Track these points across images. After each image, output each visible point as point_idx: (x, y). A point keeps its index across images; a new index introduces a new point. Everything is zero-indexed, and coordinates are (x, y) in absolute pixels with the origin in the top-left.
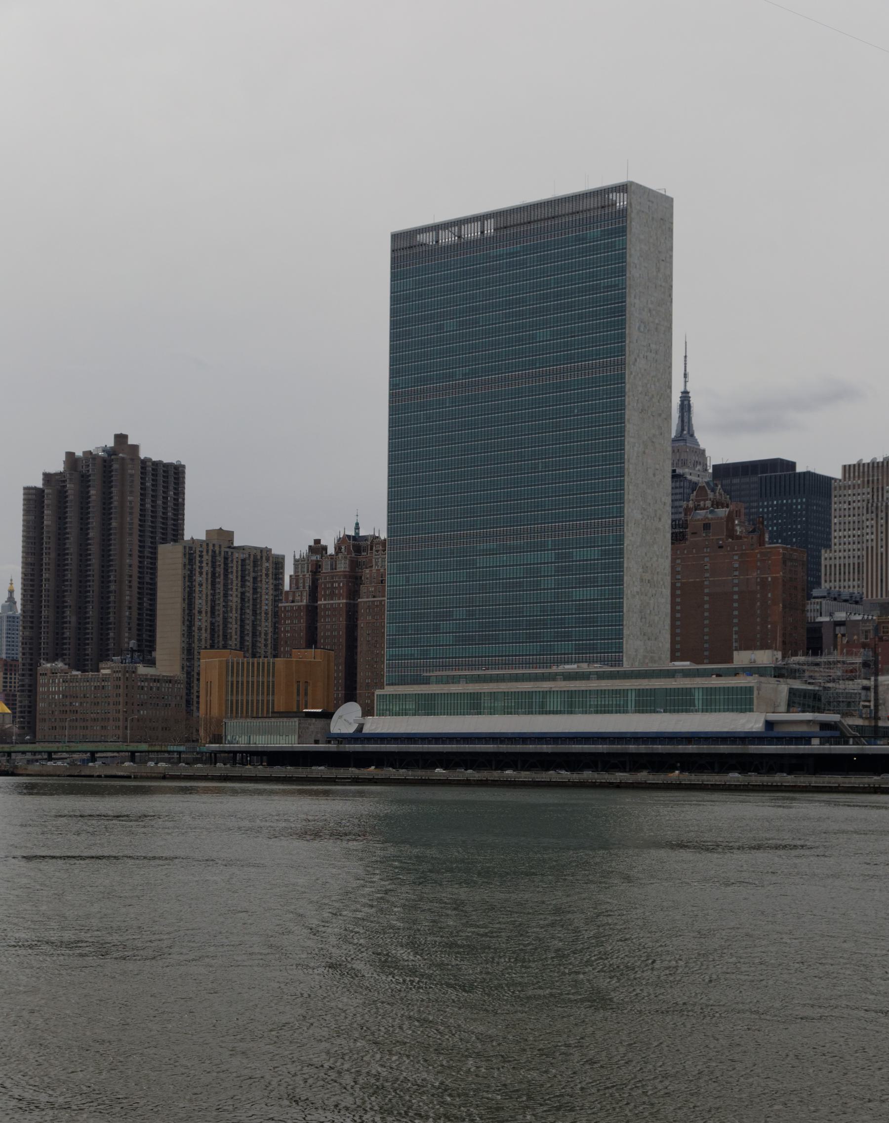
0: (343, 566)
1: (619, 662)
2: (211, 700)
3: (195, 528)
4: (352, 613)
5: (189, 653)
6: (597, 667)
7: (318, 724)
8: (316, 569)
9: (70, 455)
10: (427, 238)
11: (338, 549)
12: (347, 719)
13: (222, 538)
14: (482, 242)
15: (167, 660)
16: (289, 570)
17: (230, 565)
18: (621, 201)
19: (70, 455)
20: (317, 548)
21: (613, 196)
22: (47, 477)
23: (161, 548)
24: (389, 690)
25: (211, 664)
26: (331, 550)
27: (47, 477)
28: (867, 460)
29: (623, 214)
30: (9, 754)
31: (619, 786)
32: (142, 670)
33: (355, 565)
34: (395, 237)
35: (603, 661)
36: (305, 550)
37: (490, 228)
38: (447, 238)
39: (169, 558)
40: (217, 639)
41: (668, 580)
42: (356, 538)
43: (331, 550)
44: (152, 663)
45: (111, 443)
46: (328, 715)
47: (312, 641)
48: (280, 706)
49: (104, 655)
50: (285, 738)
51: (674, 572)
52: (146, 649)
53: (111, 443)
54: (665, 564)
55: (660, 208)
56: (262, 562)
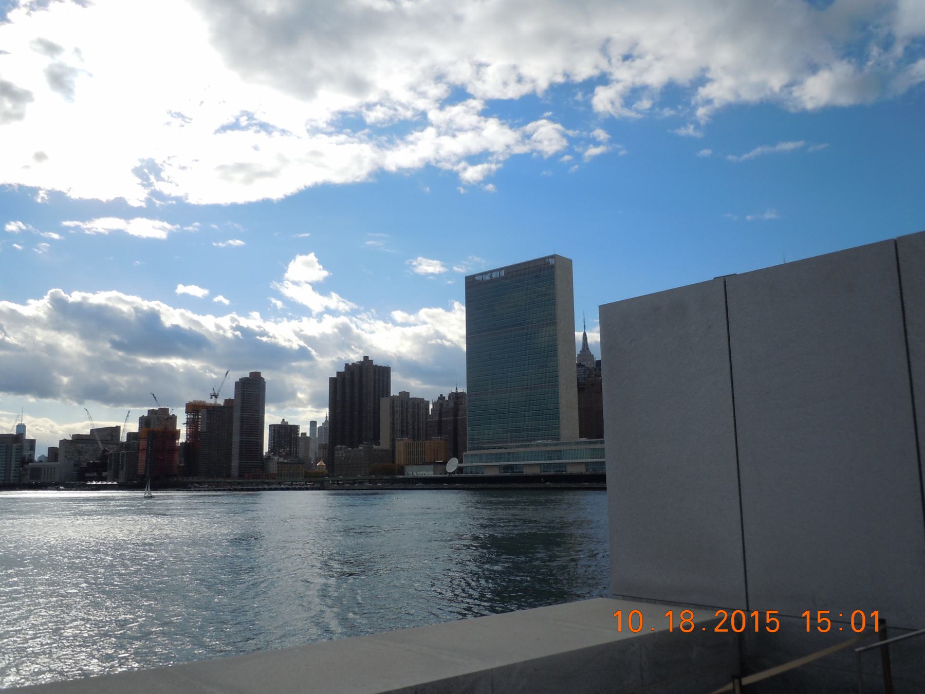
0: (452, 404)
1: (558, 439)
2: (400, 458)
3: (394, 392)
4: (455, 422)
5: (393, 441)
6: (550, 441)
7: (440, 467)
8: (441, 405)
9: (347, 365)
10: (479, 278)
11: (449, 397)
12: (452, 465)
13: (404, 395)
14: (500, 278)
15: (385, 443)
16: (431, 407)
17: (409, 406)
18: (552, 261)
19: (347, 365)
20: (441, 398)
21: (549, 260)
22: (338, 373)
23: (382, 399)
24: (468, 452)
25: (400, 445)
26: (447, 399)
27: (338, 373)
28: (302, 187)
29: (553, 267)
30: (322, 482)
31: (521, 489)
32: (375, 447)
33: (456, 404)
34: (467, 278)
35: (553, 439)
36: (436, 399)
37: (503, 273)
38: (486, 278)
39: (385, 404)
40: (404, 433)
41: (577, 407)
42: (457, 393)
43: (447, 399)
44: (379, 444)
45: (362, 360)
46: (445, 463)
47: (440, 432)
48: (427, 460)
49: (361, 442)
50: (428, 472)
51: (580, 403)
52: (376, 439)
53: (362, 360)
54: (576, 400)
55: (567, 264)
56: (420, 404)
